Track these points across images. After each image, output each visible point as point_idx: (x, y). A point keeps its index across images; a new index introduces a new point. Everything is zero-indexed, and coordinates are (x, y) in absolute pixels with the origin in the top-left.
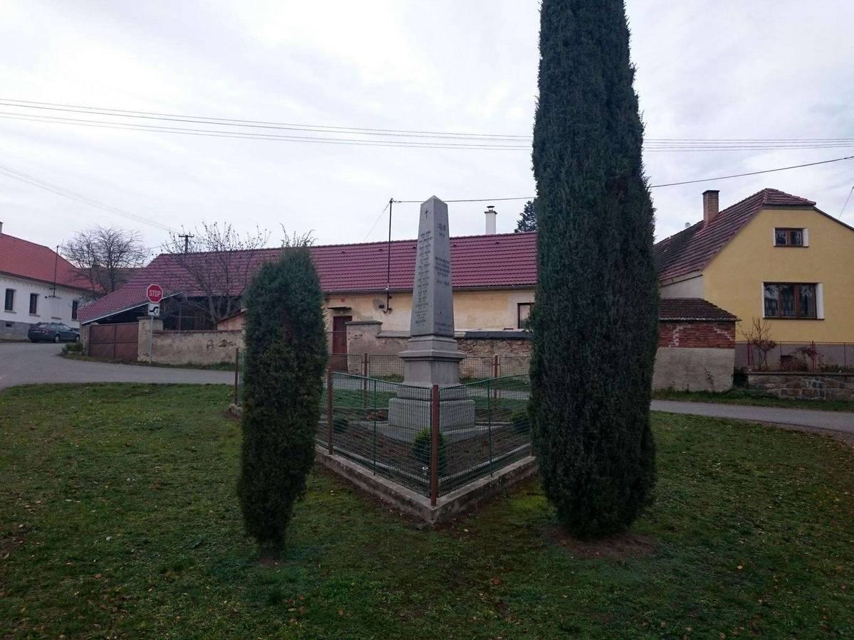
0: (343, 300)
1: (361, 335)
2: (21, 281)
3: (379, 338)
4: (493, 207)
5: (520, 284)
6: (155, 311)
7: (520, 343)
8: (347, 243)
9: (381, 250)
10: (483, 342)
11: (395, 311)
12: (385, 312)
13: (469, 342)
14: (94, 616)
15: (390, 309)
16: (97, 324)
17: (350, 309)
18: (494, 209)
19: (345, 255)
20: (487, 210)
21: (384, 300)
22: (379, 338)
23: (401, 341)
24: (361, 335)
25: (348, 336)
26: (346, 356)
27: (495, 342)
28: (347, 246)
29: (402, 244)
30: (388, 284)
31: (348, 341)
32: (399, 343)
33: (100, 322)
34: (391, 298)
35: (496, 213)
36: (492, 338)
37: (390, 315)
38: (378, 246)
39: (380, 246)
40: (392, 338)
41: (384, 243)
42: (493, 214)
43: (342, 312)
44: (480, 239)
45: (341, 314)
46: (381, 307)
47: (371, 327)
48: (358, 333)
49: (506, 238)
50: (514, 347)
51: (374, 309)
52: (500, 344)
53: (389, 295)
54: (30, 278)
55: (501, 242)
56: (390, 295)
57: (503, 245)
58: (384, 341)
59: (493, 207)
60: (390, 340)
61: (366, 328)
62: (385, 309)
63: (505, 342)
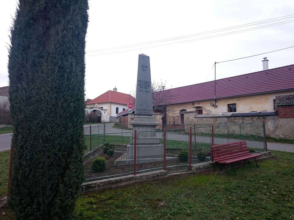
0: (199, 104)
1: (189, 117)
2: (118, 105)
3: (195, 118)
4: (266, 58)
5: (248, 94)
6: (131, 112)
7: (257, 118)
8: (207, 82)
9: (203, 86)
10: (239, 118)
11: (218, 107)
12: (215, 108)
13: (232, 118)
14: (66, 123)
15: (217, 106)
16: (122, 116)
17: (202, 107)
18: (267, 59)
19: (203, 86)
20: (264, 60)
21: (214, 103)
22: (195, 118)
23: (204, 119)
24: (189, 117)
25: (185, 117)
26: (184, 125)
27: (244, 117)
28: (248, 74)
29: (223, 80)
30: (215, 96)
31: (185, 120)
32: (203, 120)
33: (123, 116)
34: (217, 101)
35: (268, 61)
36: (243, 116)
37: (217, 109)
38: (245, 76)
39: (247, 75)
40: (200, 117)
41: (213, 81)
42: (266, 61)
43: (199, 109)
44: (256, 73)
45: (198, 109)
46: (213, 105)
47: (192, 114)
48: (188, 116)
49: (252, 74)
50: (254, 120)
51: (210, 107)
52: (247, 118)
53: (216, 100)
54: (120, 104)
55: (231, 80)
56: (216, 100)
57: (204, 86)
58: (197, 119)
59: (266, 58)
60: (200, 118)
61: (191, 114)
62: (215, 106)
63: (249, 118)
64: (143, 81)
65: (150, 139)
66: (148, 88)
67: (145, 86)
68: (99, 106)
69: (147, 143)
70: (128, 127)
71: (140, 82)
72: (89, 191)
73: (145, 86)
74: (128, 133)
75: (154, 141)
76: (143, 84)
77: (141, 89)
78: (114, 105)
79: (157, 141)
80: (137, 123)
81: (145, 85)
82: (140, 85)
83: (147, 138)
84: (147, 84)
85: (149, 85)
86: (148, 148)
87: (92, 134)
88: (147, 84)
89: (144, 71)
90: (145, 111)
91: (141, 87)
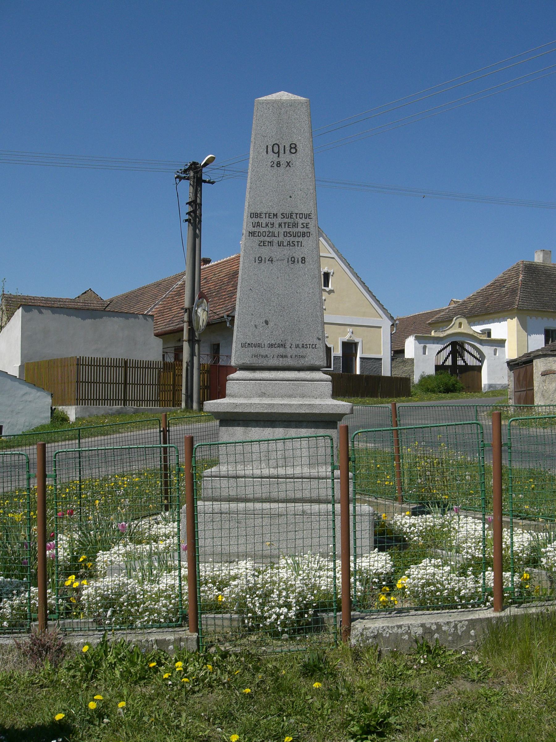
64: (275, 215)
65: (80, 474)
66: (300, 244)
67: (286, 234)
68: (472, 327)
69: (264, 496)
70: (218, 421)
71: (257, 220)
72: (290, 680)
73: (286, 234)
74: (239, 448)
75: (290, 486)
76: (276, 230)
77: (265, 252)
78: (534, 318)
79: (298, 486)
80: (290, 405)
81: (282, 230)
82: (260, 234)
83: (290, 471)
84: (295, 225)
85: (305, 230)
86: (258, 521)
87: (77, 441)
88: (295, 225)
89: (282, 170)
90: (281, 351)
91: (262, 244)
